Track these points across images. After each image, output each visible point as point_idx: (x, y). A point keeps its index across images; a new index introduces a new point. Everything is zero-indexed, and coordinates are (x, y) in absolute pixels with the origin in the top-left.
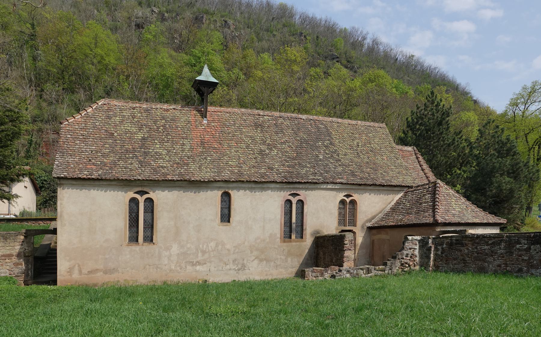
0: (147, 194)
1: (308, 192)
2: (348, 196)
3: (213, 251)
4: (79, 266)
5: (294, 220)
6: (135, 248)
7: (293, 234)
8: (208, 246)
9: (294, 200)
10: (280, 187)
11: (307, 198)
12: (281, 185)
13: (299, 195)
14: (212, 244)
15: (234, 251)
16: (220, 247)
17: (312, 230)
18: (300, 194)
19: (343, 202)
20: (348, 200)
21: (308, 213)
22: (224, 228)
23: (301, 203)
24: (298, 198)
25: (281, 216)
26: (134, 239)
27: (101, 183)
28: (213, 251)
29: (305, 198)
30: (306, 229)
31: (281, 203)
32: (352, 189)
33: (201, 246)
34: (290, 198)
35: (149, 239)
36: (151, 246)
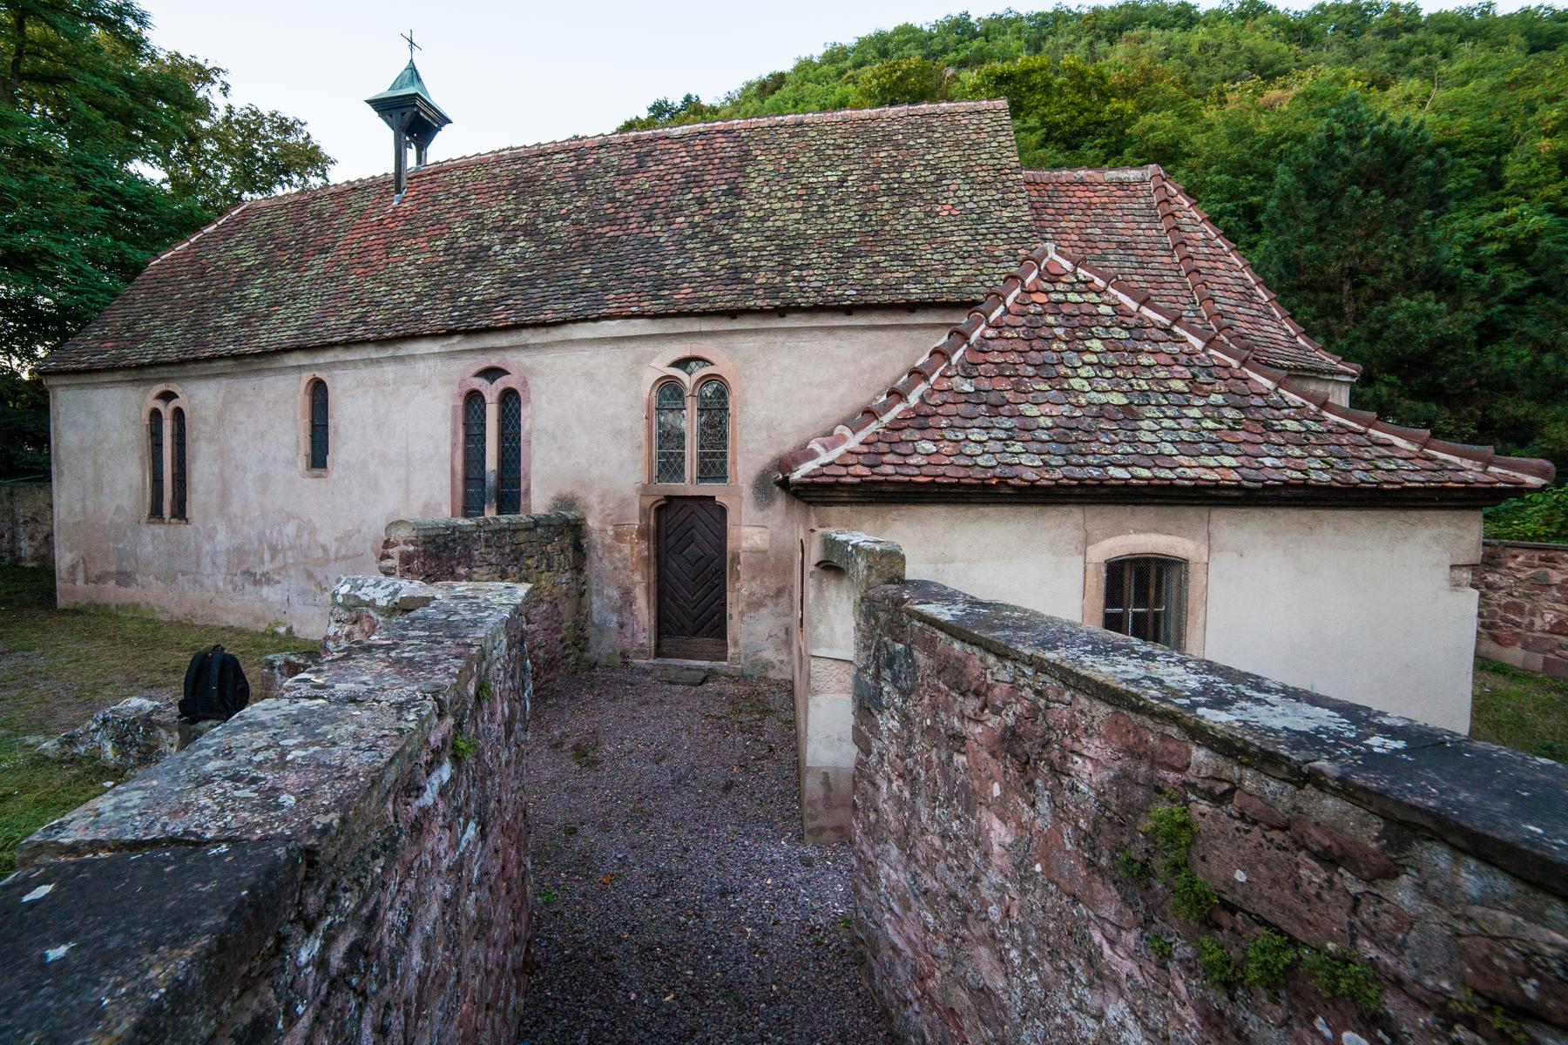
0: (505, 378)
1: (749, 346)
2: (167, 396)
3: (291, 548)
4: (84, 562)
5: (491, 463)
6: (159, 529)
7: (490, 507)
8: (280, 533)
9: (491, 392)
10: (443, 350)
11: (530, 382)
12: (445, 343)
13: (503, 372)
14: (290, 529)
15: (338, 551)
16: (305, 538)
17: (552, 494)
18: (713, 361)
19: (669, 391)
20: (687, 380)
21: (535, 434)
22: (310, 485)
23: (510, 399)
24: (501, 383)
25: (454, 445)
26: (156, 512)
27: (790, 322)
28: (291, 548)
29: (525, 383)
30: (528, 490)
31: (451, 404)
32: (701, 334)
33: (268, 532)
34: (480, 384)
35: (180, 512)
36: (183, 527)
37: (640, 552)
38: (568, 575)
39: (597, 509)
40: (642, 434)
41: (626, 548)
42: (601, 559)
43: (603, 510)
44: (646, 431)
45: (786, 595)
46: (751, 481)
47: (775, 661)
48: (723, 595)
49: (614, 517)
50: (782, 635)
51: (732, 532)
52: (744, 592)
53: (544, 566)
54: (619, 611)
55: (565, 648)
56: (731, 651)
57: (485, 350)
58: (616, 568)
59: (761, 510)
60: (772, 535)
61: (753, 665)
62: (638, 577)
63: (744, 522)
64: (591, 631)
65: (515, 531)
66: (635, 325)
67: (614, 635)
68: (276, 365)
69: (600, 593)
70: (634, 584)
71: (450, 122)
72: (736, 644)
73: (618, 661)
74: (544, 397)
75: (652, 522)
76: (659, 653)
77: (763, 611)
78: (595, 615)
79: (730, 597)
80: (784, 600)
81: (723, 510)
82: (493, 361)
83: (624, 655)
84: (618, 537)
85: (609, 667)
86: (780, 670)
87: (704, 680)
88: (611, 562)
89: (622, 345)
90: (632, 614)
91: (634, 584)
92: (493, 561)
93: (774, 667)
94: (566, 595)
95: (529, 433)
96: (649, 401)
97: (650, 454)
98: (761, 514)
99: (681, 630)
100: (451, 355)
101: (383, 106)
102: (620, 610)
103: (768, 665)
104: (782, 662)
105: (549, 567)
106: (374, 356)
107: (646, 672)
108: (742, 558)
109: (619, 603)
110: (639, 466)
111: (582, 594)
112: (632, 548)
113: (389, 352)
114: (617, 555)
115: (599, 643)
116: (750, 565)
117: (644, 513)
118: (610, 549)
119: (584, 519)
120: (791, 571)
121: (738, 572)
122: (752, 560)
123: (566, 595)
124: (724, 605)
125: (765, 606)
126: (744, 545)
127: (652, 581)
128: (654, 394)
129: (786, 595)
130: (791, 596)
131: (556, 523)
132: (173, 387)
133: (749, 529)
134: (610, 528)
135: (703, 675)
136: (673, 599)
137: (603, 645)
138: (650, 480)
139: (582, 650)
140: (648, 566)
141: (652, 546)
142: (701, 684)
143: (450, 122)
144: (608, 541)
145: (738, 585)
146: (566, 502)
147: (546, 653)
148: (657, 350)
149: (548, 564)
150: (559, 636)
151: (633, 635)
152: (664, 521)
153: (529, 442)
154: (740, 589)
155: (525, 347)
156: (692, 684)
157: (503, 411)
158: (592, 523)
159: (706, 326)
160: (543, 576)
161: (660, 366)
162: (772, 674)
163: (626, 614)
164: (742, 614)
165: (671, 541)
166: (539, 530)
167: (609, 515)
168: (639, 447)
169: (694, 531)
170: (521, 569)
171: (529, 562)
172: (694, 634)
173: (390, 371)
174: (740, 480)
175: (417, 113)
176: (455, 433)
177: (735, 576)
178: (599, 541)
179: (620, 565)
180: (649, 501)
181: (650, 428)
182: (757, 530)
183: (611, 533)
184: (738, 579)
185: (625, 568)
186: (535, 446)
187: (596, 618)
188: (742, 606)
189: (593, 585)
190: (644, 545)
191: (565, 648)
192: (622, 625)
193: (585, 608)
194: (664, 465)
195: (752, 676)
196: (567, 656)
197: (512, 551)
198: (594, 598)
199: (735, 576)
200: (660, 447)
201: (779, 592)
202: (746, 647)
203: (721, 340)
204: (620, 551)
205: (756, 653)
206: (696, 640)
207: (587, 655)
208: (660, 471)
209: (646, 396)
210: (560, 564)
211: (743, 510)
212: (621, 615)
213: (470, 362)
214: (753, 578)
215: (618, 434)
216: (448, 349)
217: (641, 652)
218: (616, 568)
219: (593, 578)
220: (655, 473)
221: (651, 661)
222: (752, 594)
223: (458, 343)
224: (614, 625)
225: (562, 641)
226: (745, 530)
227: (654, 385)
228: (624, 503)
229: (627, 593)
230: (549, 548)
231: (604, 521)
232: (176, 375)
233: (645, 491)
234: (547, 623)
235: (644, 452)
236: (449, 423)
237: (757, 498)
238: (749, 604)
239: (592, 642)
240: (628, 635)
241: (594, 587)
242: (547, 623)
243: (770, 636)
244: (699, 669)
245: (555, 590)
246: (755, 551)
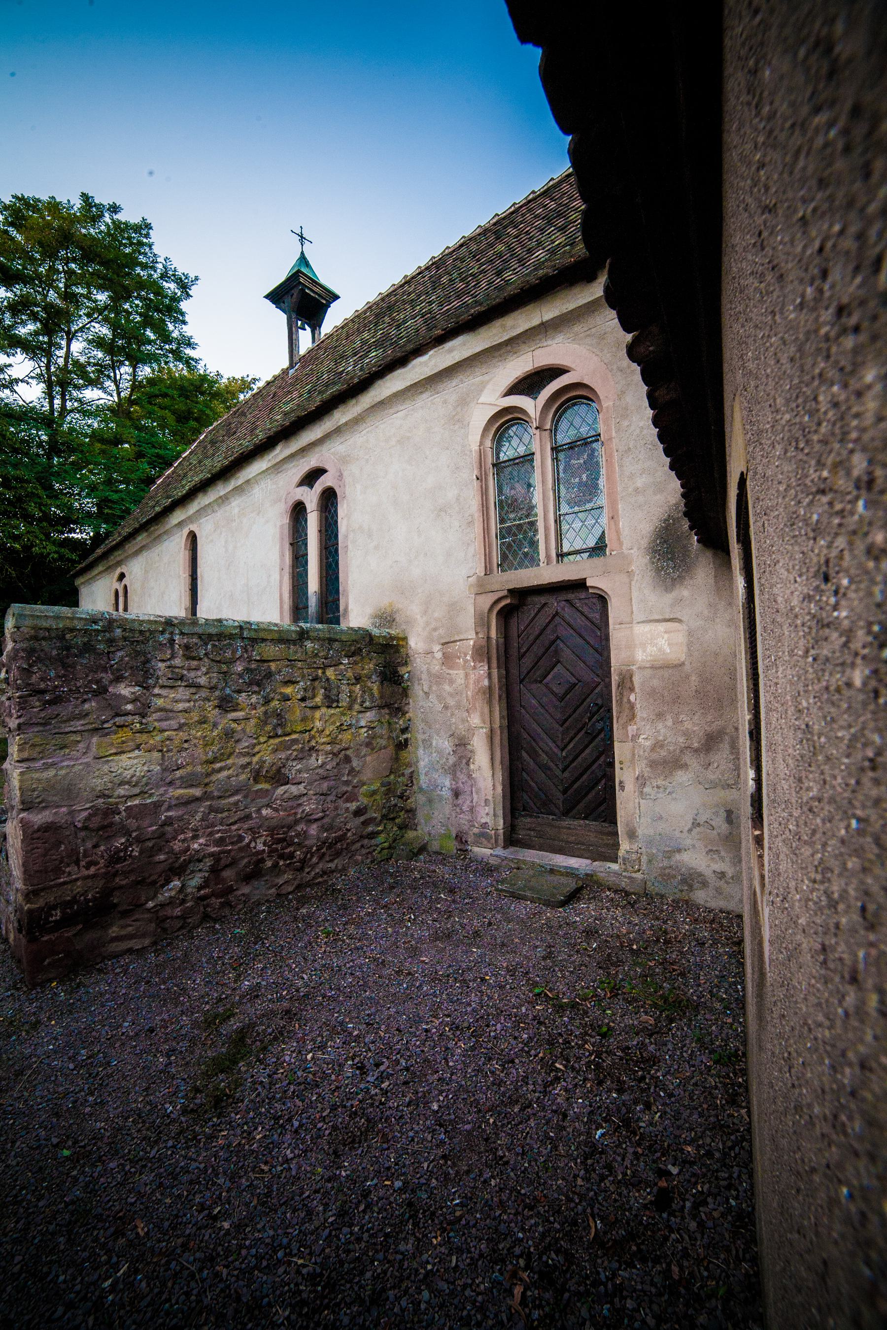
10: (269, 465)
11: (345, 474)
21: (351, 536)
23: (329, 498)
30: (346, 610)
37: (478, 681)
38: (370, 715)
39: (421, 620)
40: (473, 504)
41: (458, 675)
42: (427, 694)
43: (427, 623)
44: (478, 498)
45: (726, 746)
46: (644, 543)
47: (708, 873)
48: (608, 749)
49: (441, 631)
50: (720, 822)
51: (617, 635)
52: (645, 742)
53: (318, 699)
54: (453, 771)
55: (365, 823)
56: (625, 846)
57: (304, 451)
58: (446, 707)
59: (668, 589)
60: (690, 633)
61: (666, 876)
62: (475, 720)
63: (638, 616)
64: (418, 800)
65: (254, 641)
66: (451, 351)
67: (447, 809)
68: (168, 527)
69: (427, 744)
70: (471, 730)
71: (336, 297)
72: (632, 835)
73: (452, 846)
74: (358, 487)
75: (493, 634)
76: (511, 839)
77: (681, 777)
78: (422, 777)
79: (620, 751)
80: (721, 757)
81: (602, 600)
82: (311, 462)
83: (460, 838)
84: (448, 660)
85: (441, 857)
86: (719, 891)
87: (573, 897)
88: (440, 698)
89: (441, 386)
90: (470, 776)
91: (471, 730)
92: (203, 681)
93: (704, 884)
94: (368, 744)
95: (346, 537)
96: (481, 455)
97: (486, 530)
98: (669, 598)
99: (545, 805)
100: (277, 467)
101: (276, 297)
102: (453, 771)
103: (691, 880)
104: (722, 875)
105: (331, 701)
106: (222, 493)
107: (488, 869)
108: (637, 680)
109: (452, 760)
110: (471, 550)
111: (402, 746)
112: (467, 675)
113: (233, 483)
114: (447, 687)
115: (429, 818)
116: (652, 693)
117: (482, 622)
118: (438, 679)
119: (405, 639)
120: (734, 701)
121: (632, 707)
122: (655, 683)
123: (368, 744)
124: (612, 765)
125: (684, 766)
126: (641, 656)
127: (497, 725)
128: (488, 443)
129: (726, 746)
130: (734, 746)
131: (344, 638)
132: (123, 569)
133: (647, 628)
134: (436, 648)
135: (572, 885)
136: (534, 755)
137: (435, 822)
138: (488, 571)
139: (403, 827)
140: (490, 702)
141: (495, 672)
142: (563, 904)
143: (336, 297)
144: (436, 668)
145: (632, 729)
146: (387, 618)
147: (323, 828)
148: (486, 377)
149: (327, 697)
150: (353, 806)
151: (472, 809)
152: (514, 632)
153: (346, 547)
154: (635, 737)
155: (338, 431)
156: (548, 904)
157: (327, 518)
158: (416, 643)
159: (548, 311)
160: (318, 714)
161: (492, 400)
162: (700, 896)
163: (462, 777)
164: (641, 781)
165: (528, 661)
166: (309, 645)
167: (435, 629)
168: (470, 523)
169: (558, 641)
170: (267, 701)
171: (288, 690)
172: (566, 813)
173: (236, 505)
174: (626, 543)
175: (303, 290)
176: (282, 555)
177: (626, 712)
178: (424, 668)
179: (451, 702)
180: (489, 599)
181: (484, 493)
182: (662, 627)
183: (439, 655)
184: (633, 717)
185: (458, 706)
186: (350, 554)
187: (423, 781)
188: (641, 767)
189: (418, 734)
190: (483, 670)
191: (365, 823)
192: (457, 794)
193: (409, 765)
194: (509, 546)
195: (662, 896)
196: (373, 835)
197: (248, 670)
198: (421, 752)
199: (626, 712)
200: (502, 521)
201: (711, 742)
202: (650, 842)
203: (577, 328)
204: (451, 682)
205: (669, 855)
206: (566, 822)
207: (410, 834)
208: (504, 557)
209: (475, 447)
210: (353, 700)
211: (635, 594)
212: (455, 778)
213: (294, 471)
214: (660, 716)
215: (441, 511)
216: (273, 462)
217: (483, 836)
218: (446, 707)
219: (418, 725)
220: (496, 558)
221: (499, 851)
222: (658, 745)
223: (281, 451)
224: (446, 793)
225: (358, 812)
226: (641, 630)
227: (483, 435)
228: (454, 608)
229: (462, 744)
230: (330, 673)
231: (430, 639)
232: (122, 557)
233: (481, 589)
234: (325, 785)
235: (478, 528)
236: (278, 547)
237: (658, 570)
238: (653, 764)
239: (420, 816)
240: (465, 808)
241: (420, 737)
242: (325, 785)
243: (696, 824)
244: (570, 873)
245: (346, 736)
246: (659, 667)
